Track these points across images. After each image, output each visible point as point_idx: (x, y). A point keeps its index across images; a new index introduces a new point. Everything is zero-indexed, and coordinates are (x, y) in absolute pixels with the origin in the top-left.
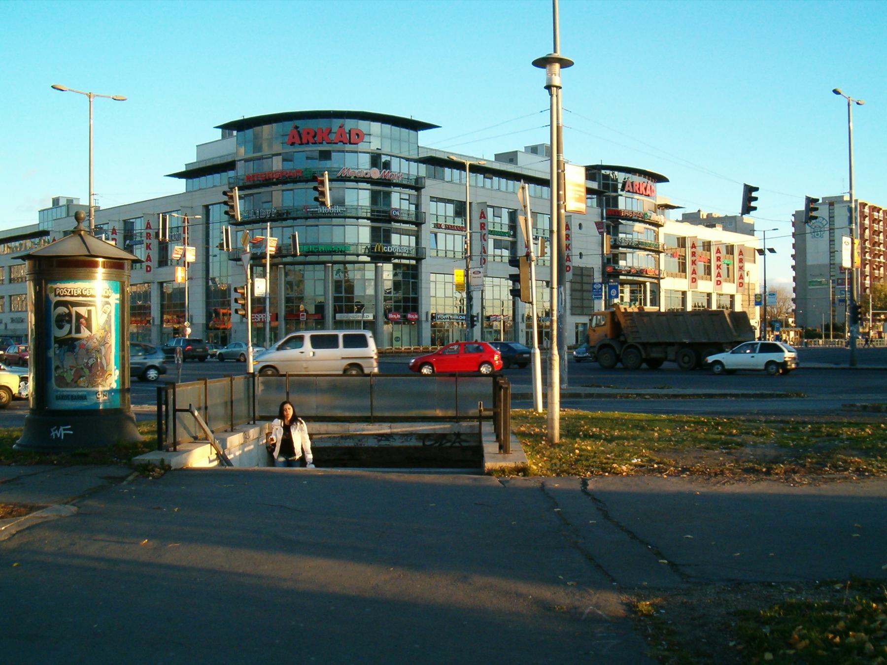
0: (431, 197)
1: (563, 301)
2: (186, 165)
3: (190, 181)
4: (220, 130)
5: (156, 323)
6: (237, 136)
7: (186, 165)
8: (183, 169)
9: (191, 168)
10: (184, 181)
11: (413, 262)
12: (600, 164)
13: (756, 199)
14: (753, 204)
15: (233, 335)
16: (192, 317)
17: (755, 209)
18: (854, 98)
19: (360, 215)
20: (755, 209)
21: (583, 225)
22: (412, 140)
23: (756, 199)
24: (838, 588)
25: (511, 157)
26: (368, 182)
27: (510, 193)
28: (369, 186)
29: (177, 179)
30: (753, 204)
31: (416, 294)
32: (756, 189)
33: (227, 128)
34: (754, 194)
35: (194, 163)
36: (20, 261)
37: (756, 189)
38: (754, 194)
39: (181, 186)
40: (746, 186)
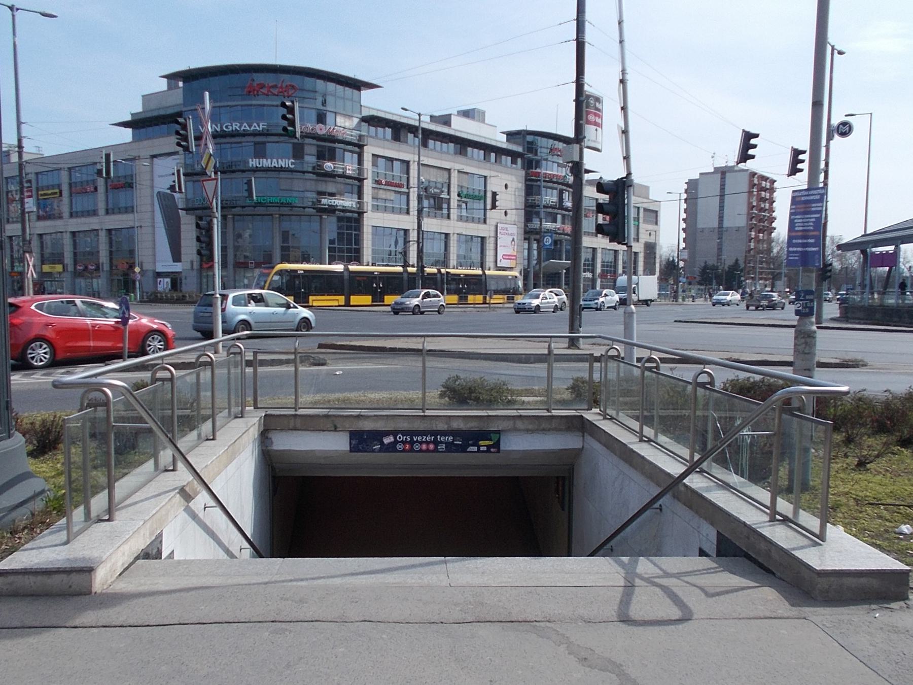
0: (373, 155)
1: (807, 220)
2: (143, 96)
3: (137, 131)
4: (165, 80)
5: (105, 269)
6: (184, 88)
7: (143, 96)
8: (128, 118)
9: (136, 118)
10: (130, 130)
11: (356, 215)
12: (525, 129)
13: (755, 146)
14: (751, 152)
15: (184, 281)
16: (142, 263)
17: (753, 157)
18: (838, 47)
19: (305, 170)
20: (753, 157)
21: (509, 185)
22: (356, 98)
23: (755, 146)
24: (906, 531)
25: (446, 120)
26: (313, 138)
27: (445, 153)
28: (315, 142)
29: (122, 129)
30: (751, 152)
31: (358, 245)
32: (756, 136)
33: (172, 78)
34: (753, 141)
35: (140, 113)
36: (122, 586)
37: (756, 136)
38: (753, 141)
39: (127, 135)
40: (744, 131)
